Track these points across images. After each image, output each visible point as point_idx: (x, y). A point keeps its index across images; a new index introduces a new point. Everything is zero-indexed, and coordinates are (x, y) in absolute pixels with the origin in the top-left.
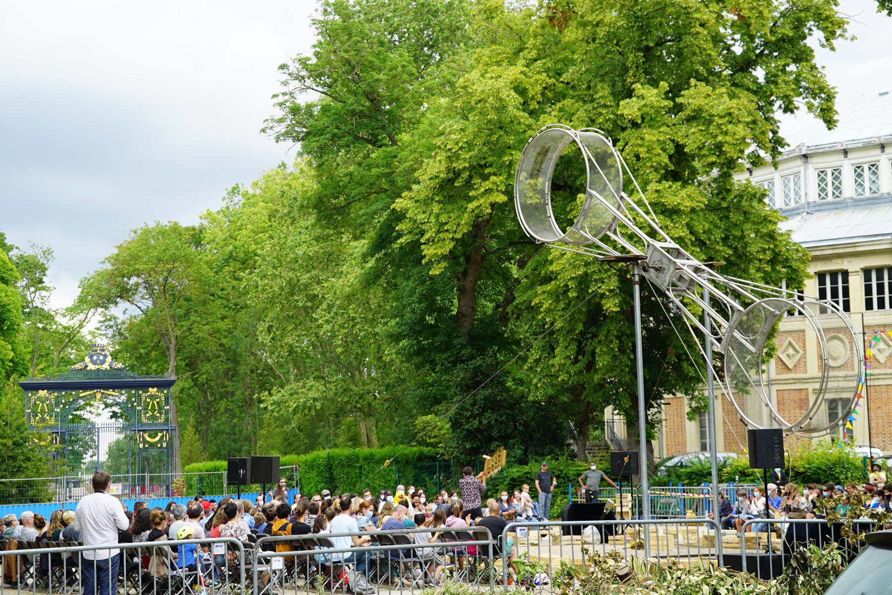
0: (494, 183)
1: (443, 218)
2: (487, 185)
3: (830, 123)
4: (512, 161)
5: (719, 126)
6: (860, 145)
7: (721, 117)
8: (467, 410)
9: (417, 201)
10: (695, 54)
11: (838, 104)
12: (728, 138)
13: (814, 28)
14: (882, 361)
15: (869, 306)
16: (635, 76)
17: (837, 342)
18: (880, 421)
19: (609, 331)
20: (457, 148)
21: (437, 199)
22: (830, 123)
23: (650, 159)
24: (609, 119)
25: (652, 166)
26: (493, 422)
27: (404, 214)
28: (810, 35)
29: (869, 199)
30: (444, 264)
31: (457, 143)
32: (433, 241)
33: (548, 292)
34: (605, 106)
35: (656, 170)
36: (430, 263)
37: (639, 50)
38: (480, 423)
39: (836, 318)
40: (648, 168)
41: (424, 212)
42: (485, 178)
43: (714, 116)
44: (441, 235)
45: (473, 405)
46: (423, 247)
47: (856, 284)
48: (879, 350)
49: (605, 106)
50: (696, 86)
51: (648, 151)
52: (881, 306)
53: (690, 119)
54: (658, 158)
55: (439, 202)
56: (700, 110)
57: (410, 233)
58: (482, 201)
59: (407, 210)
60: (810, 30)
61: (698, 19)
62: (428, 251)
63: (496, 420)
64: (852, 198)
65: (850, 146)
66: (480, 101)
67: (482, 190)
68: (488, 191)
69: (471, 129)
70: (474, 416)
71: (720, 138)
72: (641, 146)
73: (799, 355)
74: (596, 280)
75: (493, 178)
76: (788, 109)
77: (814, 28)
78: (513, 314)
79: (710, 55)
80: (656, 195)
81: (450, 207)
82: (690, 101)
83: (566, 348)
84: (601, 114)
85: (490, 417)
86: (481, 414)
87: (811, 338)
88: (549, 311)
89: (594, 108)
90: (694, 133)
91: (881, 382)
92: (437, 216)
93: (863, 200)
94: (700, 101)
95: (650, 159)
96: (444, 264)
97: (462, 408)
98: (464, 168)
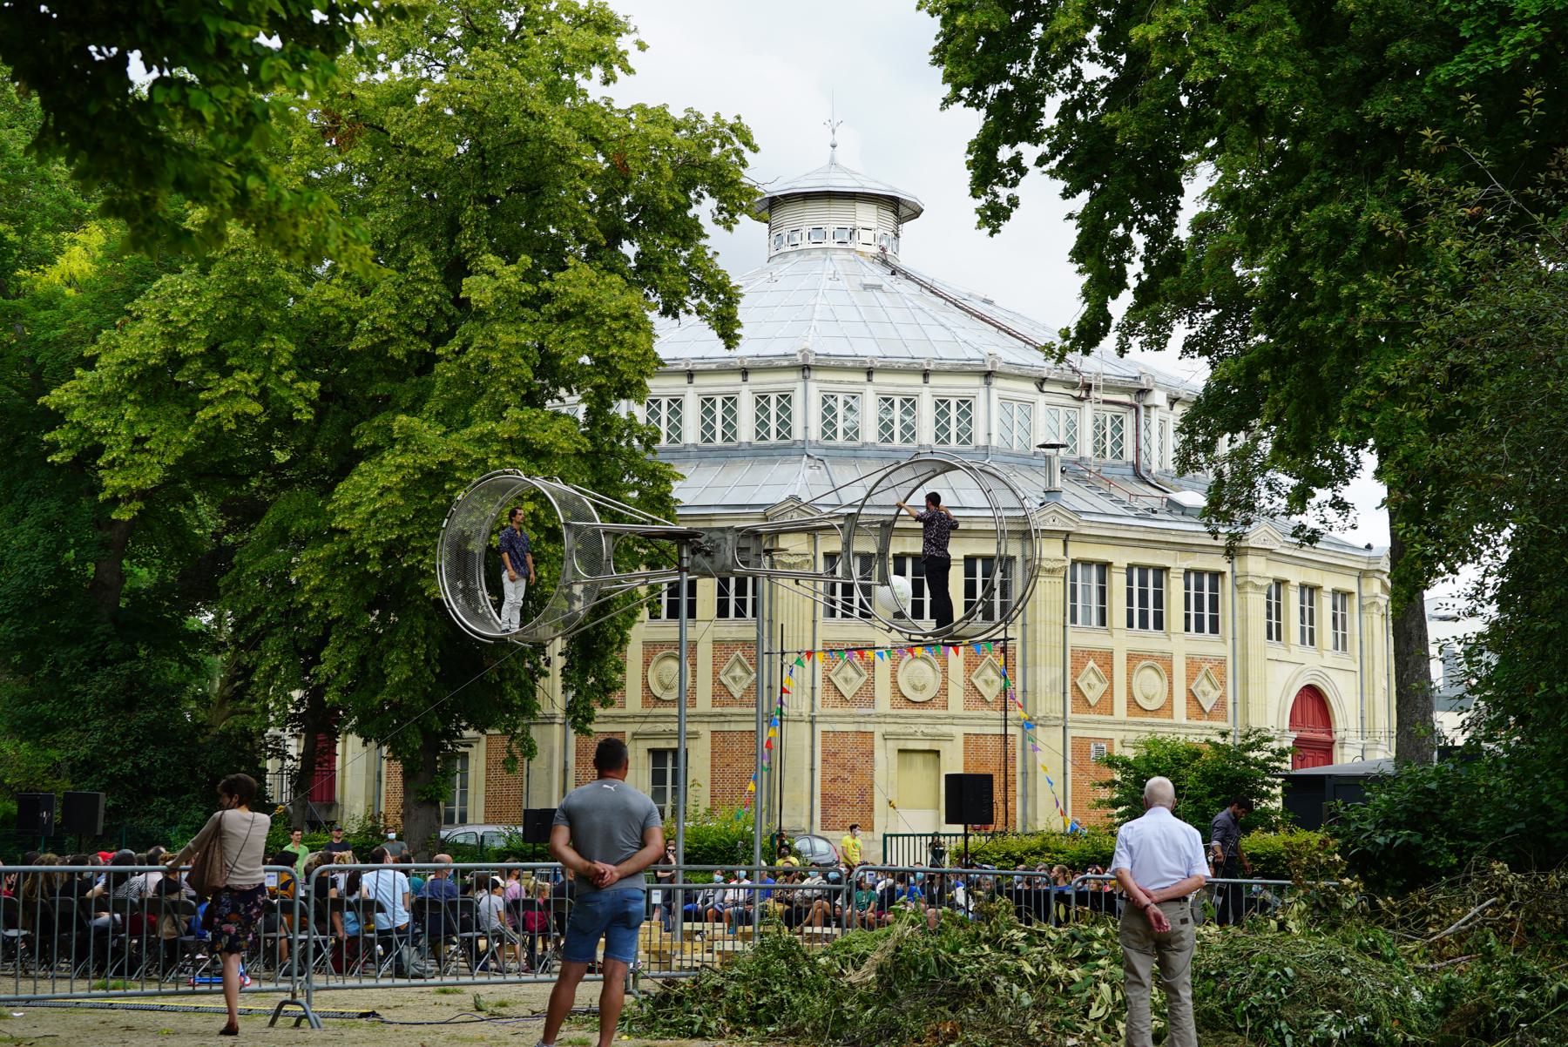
0: (243, 382)
1: (142, 430)
2: (229, 384)
3: (730, 339)
4: (273, 350)
5: (611, 332)
6: (714, 367)
7: (615, 319)
8: (114, 743)
9: (89, 398)
10: (564, 217)
11: (743, 312)
12: (626, 352)
13: (705, 194)
14: (737, 696)
15: (723, 611)
16: (473, 240)
17: (1150, 672)
18: (728, 786)
19: (412, 628)
20: (185, 321)
21: (132, 397)
22: (730, 339)
23: (506, 372)
24: (433, 302)
25: (509, 382)
26: (157, 765)
27: (62, 416)
28: (698, 202)
29: (720, 449)
30: (137, 505)
31: (187, 314)
32: (121, 464)
33: (318, 561)
34: (426, 280)
35: (515, 388)
36: (114, 501)
37: (481, 200)
38: (136, 765)
39: (1150, 640)
40: (503, 384)
41: (104, 417)
42: (227, 372)
43: (604, 316)
44: (136, 456)
45: (124, 736)
46: (101, 473)
47: (1175, 590)
48: (734, 678)
49: (426, 280)
50: (575, 267)
51: (504, 359)
52: (740, 613)
53: (563, 317)
54: (518, 371)
55: (134, 402)
56: (583, 305)
57: (69, 447)
58: (221, 409)
59: (70, 409)
60: (701, 196)
61: (578, 167)
62: (113, 482)
63: (163, 762)
64: (695, 445)
65: (698, 367)
66: (234, 252)
67: (223, 391)
68: (233, 395)
69: (208, 296)
70: (125, 754)
71: (613, 350)
72: (492, 349)
73: (864, 679)
74: (414, 549)
75: (240, 375)
76: (669, 311)
77: (705, 194)
78: (227, 590)
79: (585, 221)
80: (517, 427)
81: (152, 414)
82: (570, 290)
83: (340, 650)
84: (420, 292)
85: (152, 756)
86: (136, 752)
87: (705, 653)
88: (317, 590)
89: (407, 281)
90: (573, 338)
91: (733, 727)
92: (131, 425)
93: (711, 450)
94: (583, 292)
95: (506, 372)
96: (137, 505)
97: (107, 741)
98: (197, 356)
